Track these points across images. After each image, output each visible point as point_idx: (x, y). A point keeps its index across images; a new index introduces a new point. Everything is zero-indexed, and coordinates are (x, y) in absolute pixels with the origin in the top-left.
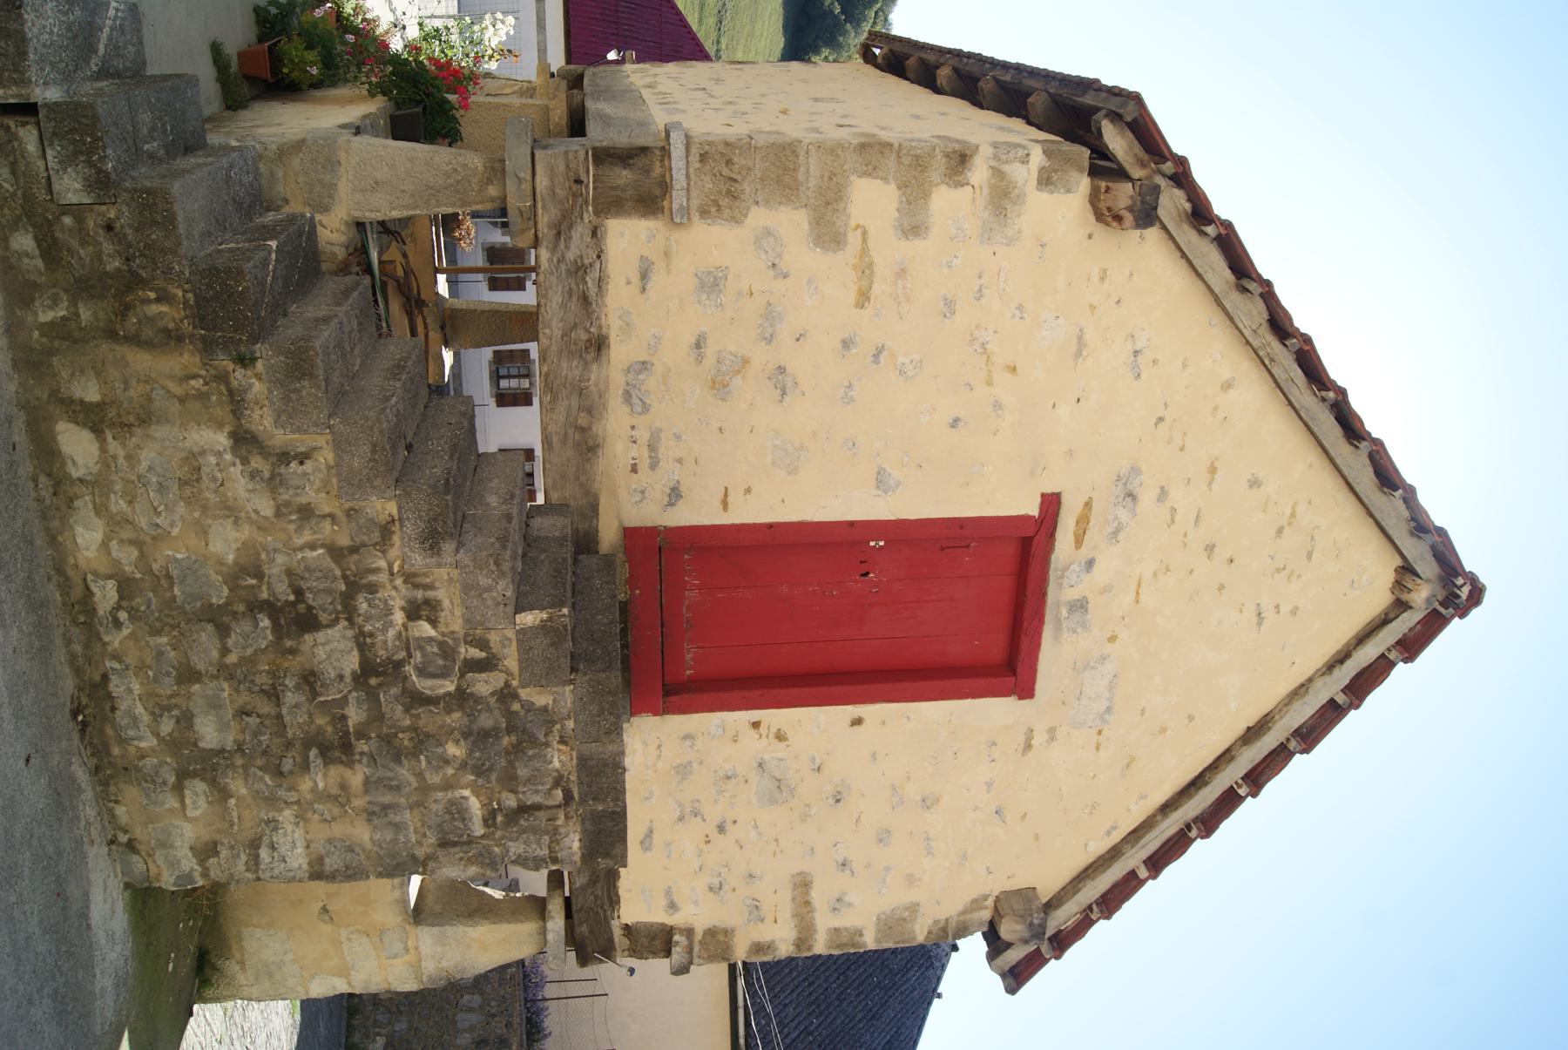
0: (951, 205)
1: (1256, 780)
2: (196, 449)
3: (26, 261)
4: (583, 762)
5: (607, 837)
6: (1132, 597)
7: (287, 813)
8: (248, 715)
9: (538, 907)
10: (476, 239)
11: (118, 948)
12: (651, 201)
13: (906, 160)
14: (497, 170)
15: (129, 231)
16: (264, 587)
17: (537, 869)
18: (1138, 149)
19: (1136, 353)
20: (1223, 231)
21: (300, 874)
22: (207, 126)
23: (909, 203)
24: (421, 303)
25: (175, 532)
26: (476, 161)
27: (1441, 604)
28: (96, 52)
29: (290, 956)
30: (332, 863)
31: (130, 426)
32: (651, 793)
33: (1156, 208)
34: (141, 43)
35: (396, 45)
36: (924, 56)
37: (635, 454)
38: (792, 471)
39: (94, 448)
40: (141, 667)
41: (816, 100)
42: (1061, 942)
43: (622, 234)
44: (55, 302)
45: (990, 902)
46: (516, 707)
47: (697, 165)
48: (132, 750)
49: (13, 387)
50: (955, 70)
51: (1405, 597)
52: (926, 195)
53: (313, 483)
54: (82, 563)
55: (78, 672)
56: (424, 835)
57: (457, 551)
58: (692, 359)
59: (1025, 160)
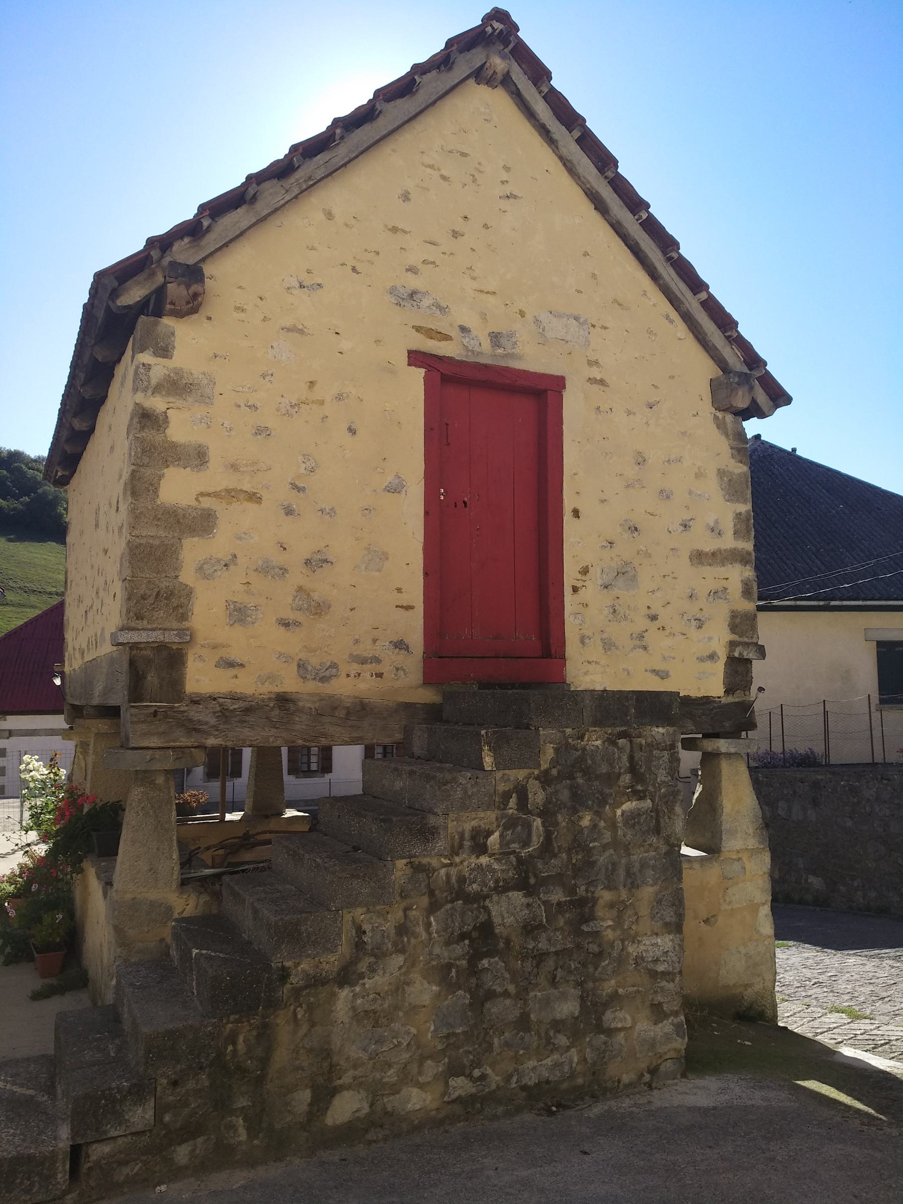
0: (182, 428)
1: (636, 204)
2: (351, 1014)
3: (198, 1151)
4: (594, 724)
5: (656, 706)
6: (491, 299)
7: (630, 949)
8: (555, 978)
9: (710, 759)
10: (200, 788)
11: (732, 1085)
12: (172, 659)
13: (146, 460)
14: (144, 777)
15: (179, 1067)
16: (458, 963)
17: (679, 760)
18: (140, 277)
19: (302, 286)
20: (207, 213)
21: (677, 941)
22: (100, 1004)
23: (180, 459)
24: (246, 836)
25: (414, 1031)
26: (136, 793)
27: (506, 46)
28: (32, 1097)
29: (742, 949)
30: (669, 915)
31: (331, 1066)
32: (624, 669)
33: (188, 266)
34: (28, 1059)
35: (41, 850)
36: (63, 439)
37: (368, 675)
38: (385, 556)
39: (347, 1094)
40: (517, 1059)
41: (97, 526)
42: (754, 361)
43: (198, 681)
44: (232, 1127)
45: (720, 415)
46: (554, 772)
47: (145, 622)
48: (579, 1068)
49: (297, 1161)
50: (75, 415)
51: (499, 77)
52: (174, 446)
53: (379, 924)
54: (435, 1105)
55: (519, 1110)
56: (650, 845)
57: (435, 814)
58: (297, 630)
59: (147, 367)
